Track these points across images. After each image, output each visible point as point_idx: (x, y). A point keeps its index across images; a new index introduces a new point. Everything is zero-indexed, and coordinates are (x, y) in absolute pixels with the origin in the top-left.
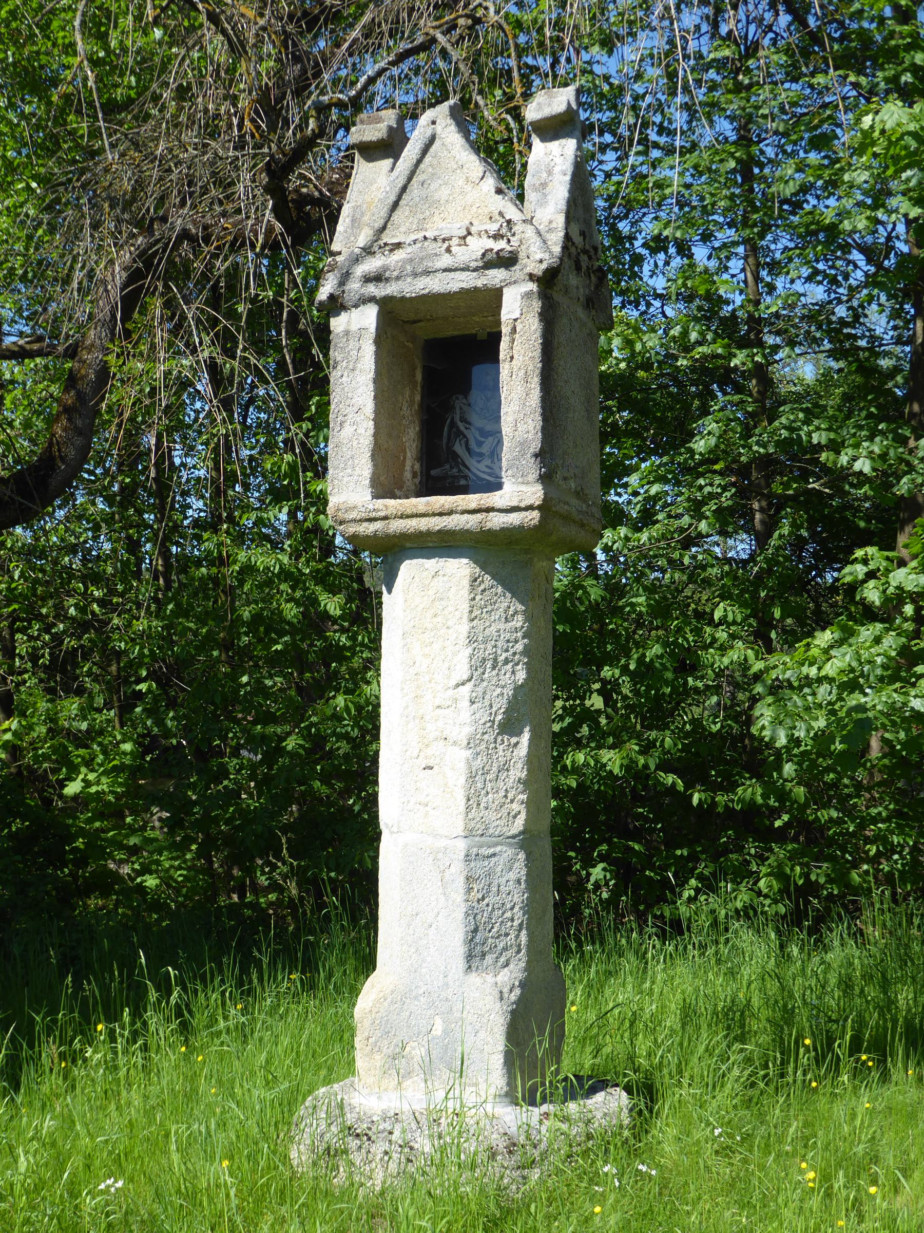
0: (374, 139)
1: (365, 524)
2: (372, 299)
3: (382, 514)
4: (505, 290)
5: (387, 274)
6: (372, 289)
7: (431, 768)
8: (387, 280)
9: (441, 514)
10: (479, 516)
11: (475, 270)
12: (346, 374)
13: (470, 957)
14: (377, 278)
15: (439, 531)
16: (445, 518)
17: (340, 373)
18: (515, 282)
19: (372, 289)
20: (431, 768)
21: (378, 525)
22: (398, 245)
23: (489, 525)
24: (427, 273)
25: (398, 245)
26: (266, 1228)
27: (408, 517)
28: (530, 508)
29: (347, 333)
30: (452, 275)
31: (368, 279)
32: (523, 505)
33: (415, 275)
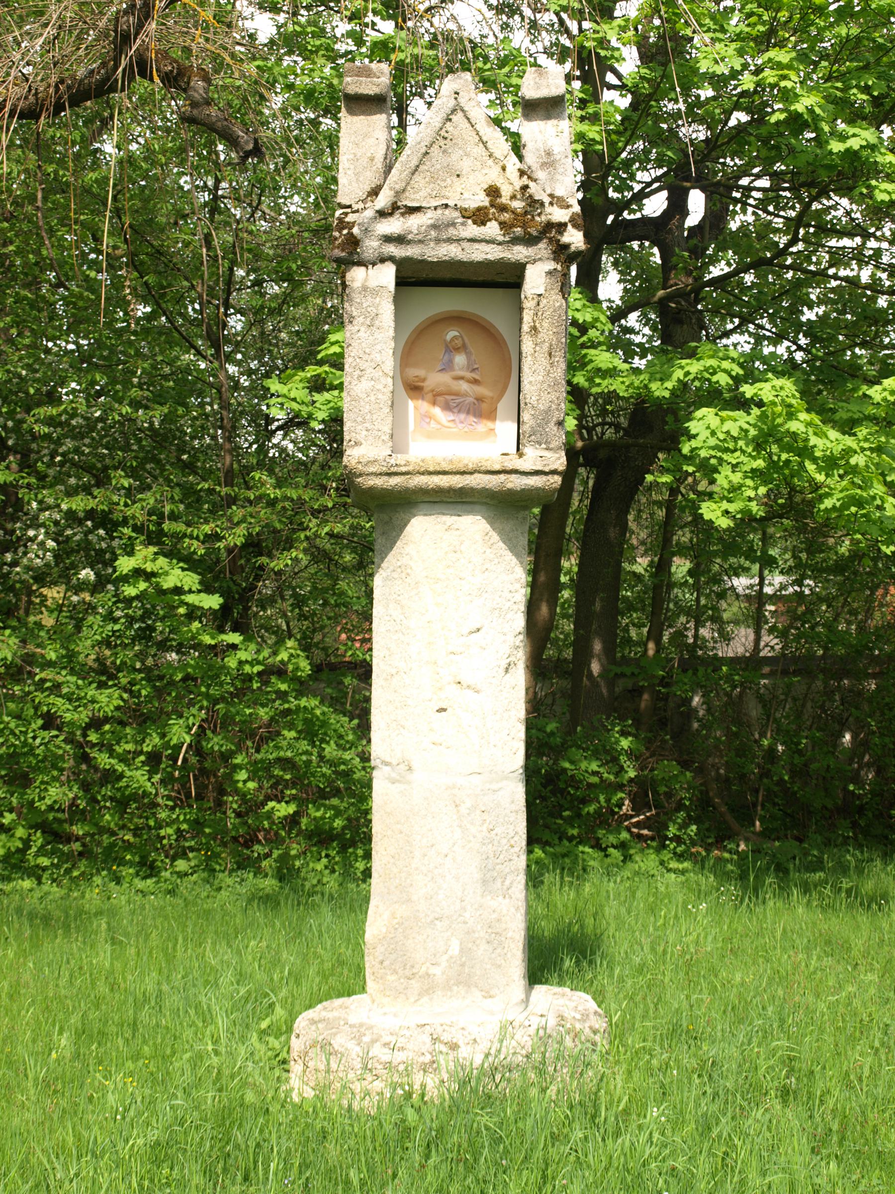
0: (371, 93)
1: (385, 478)
2: (392, 259)
3: (404, 469)
4: (528, 266)
5: (410, 237)
6: (392, 249)
7: (444, 710)
8: (409, 242)
9: (463, 473)
10: (502, 477)
11: (500, 244)
12: (363, 329)
13: (484, 882)
14: (399, 240)
15: (461, 488)
16: (468, 476)
17: (357, 328)
18: (540, 259)
19: (392, 249)
20: (444, 710)
21: (394, 481)
22: (418, 209)
23: (510, 486)
24: (450, 240)
25: (418, 209)
26: (729, 1187)
27: (431, 473)
28: (554, 472)
29: (365, 288)
30: (476, 245)
31: (388, 239)
32: (547, 469)
33: (438, 241)
